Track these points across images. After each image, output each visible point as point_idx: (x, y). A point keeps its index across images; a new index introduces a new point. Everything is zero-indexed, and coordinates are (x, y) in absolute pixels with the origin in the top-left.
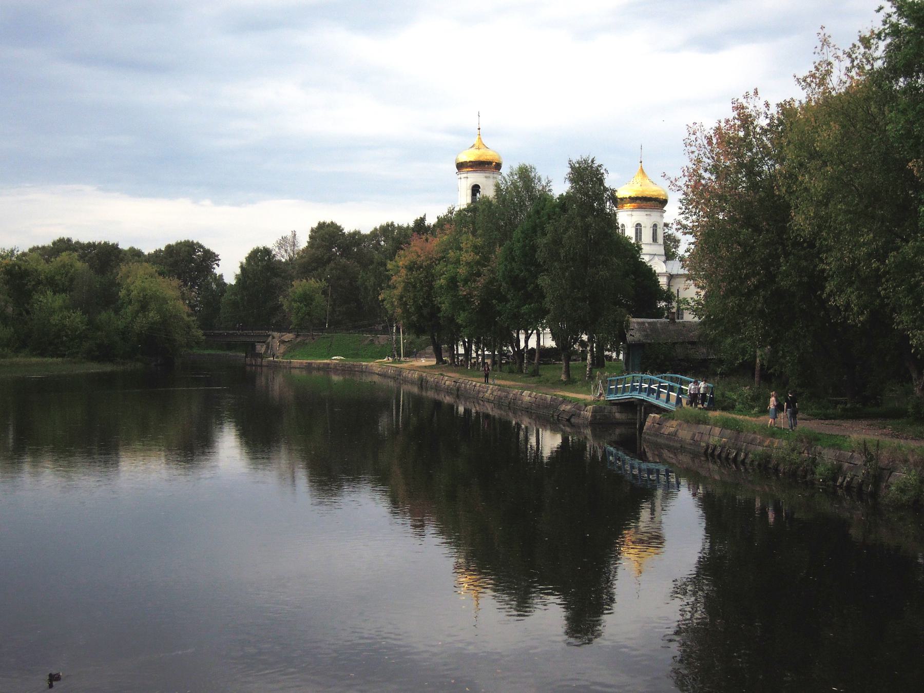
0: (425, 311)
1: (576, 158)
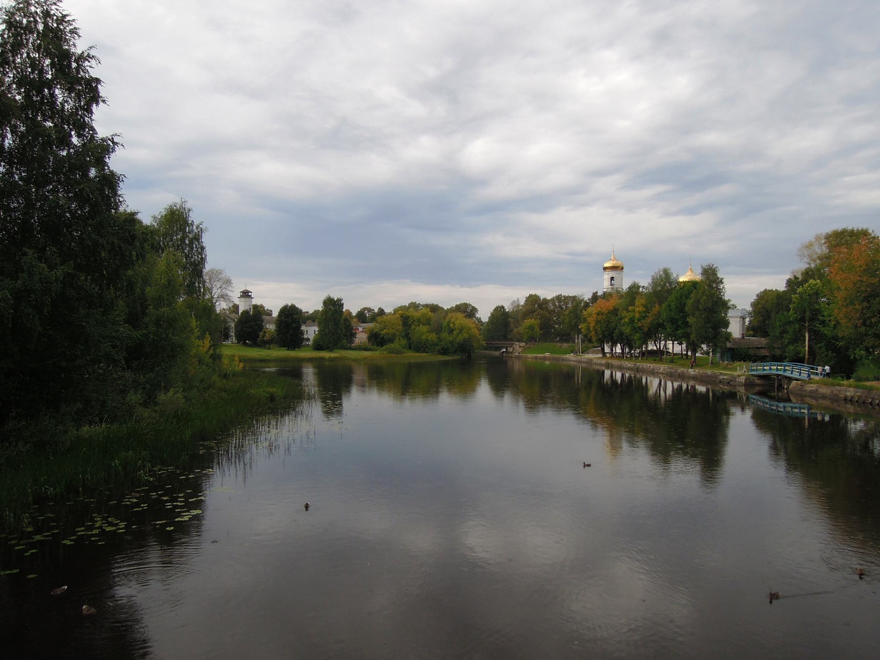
0: (606, 333)
1: (705, 265)
